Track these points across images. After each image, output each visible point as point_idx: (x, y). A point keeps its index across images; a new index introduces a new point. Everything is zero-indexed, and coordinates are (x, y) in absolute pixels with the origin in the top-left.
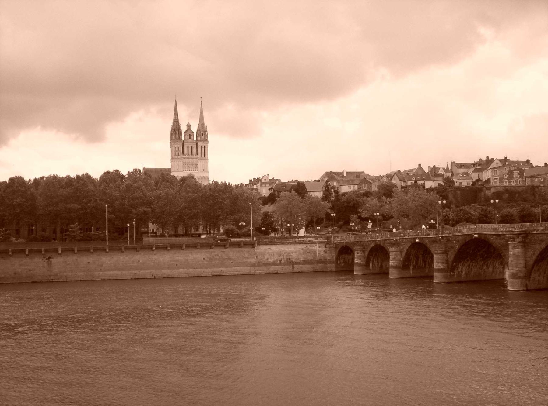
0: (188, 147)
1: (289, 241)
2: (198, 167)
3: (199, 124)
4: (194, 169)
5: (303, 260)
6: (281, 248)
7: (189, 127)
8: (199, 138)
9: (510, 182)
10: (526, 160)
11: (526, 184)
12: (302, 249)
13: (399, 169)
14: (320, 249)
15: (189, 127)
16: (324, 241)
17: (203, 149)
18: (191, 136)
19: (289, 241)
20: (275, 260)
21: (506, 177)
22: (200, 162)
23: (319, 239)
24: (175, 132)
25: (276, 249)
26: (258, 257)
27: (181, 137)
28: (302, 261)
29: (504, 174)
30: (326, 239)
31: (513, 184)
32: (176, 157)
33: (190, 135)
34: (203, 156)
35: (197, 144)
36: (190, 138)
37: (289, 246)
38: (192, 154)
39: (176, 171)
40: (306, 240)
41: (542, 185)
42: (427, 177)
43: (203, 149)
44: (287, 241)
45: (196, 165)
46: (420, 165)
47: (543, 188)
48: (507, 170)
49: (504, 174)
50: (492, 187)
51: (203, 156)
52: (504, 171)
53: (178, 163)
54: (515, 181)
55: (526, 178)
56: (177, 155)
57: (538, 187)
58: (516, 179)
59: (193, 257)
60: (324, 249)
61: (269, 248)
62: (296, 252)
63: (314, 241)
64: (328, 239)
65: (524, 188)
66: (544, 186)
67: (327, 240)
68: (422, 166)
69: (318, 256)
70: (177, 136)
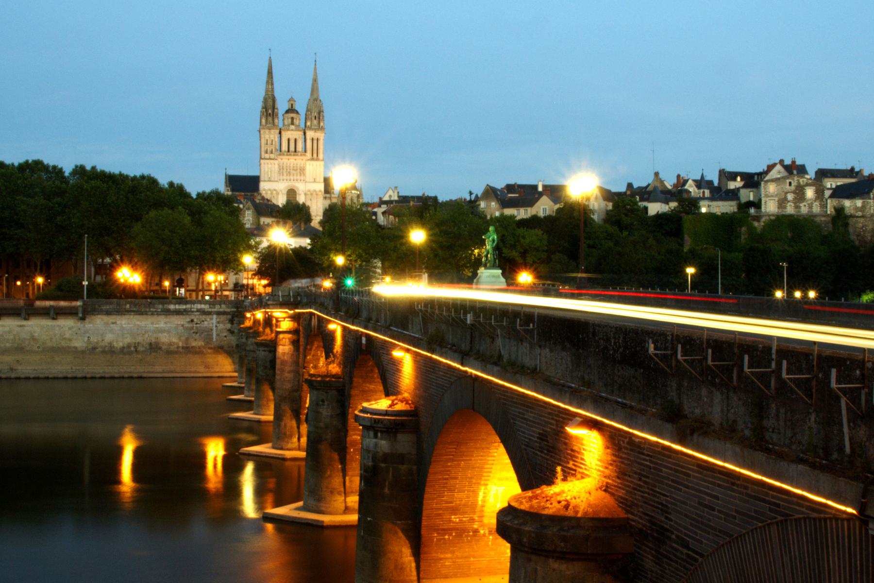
0: (289, 140)
1: (154, 310)
2: (304, 175)
3: (309, 100)
4: (299, 177)
5: (183, 348)
6: (138, 323)
7: (292, 105)
8: (309, 124)
9: (797, 207)
10: (849, 168)
11: (826, 211)
12: (183, 325)
13: (630, 182)
14: (221, 326)
15: (292, 105)
16: (229, 310)
17: (315, 142)
18: (295, 120)
19: (154, 310)
20: (741, 403)
21: (790, 197)
22: (309, 165)
23: (219, 306)
24: (267, 113)
25: (129, 324)
26: (91, 339)
27: (276, 121)
28: (180, 350)
29: (786, 193)
30: (232, 308)
31: (804, 210)
32: (267, 156)
33: (292, 118)
34: (315, 155)
35: (305, 134)
36: (292, 123)
37: (155, 318)
38: (295, 151)
39: (266, 180)
40: (191, 308)
41: (860, 214)
42: (647, 193)
43: (315, 142)
44: (152, 309)
45: (302, 171)
46: (657, 174)
47: (862, 220)
48: (794, 184)
49: (786, 193)
50: (763, 216)
51: (315, 155)
52: (788, 187)
53: (270, 166)
54: (807, 206)
55: (827, 200)
56: (268, 152)
57: (852, 216)
58: (809, 202)
59: (289, 372)
60: (229, 326)
61: (114, 321)
62: (169, 332)
63: (206, 310)
64: (237, 308)
65: (823, 219)
66: (863, 217)
67: (235, 310)
68: (661, 176)
69: (214, 340)
70: (270, 119)
